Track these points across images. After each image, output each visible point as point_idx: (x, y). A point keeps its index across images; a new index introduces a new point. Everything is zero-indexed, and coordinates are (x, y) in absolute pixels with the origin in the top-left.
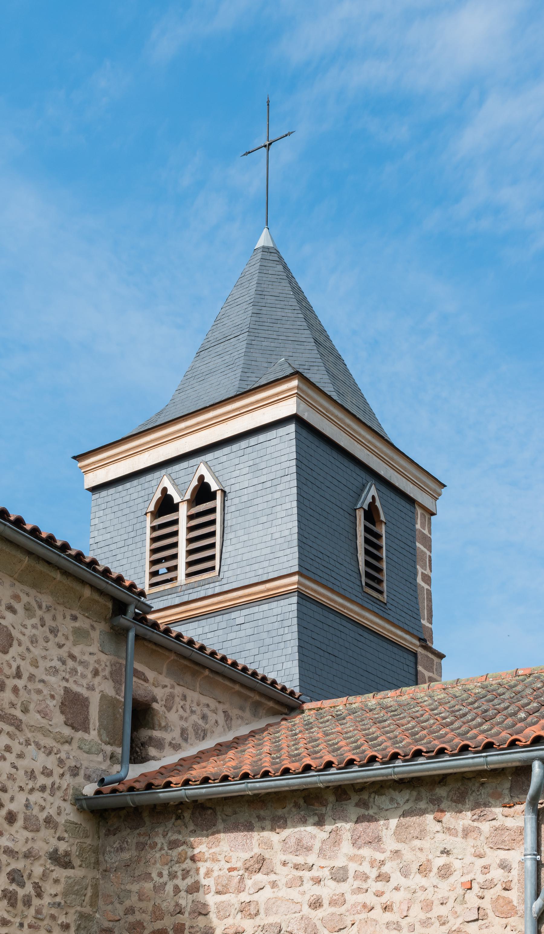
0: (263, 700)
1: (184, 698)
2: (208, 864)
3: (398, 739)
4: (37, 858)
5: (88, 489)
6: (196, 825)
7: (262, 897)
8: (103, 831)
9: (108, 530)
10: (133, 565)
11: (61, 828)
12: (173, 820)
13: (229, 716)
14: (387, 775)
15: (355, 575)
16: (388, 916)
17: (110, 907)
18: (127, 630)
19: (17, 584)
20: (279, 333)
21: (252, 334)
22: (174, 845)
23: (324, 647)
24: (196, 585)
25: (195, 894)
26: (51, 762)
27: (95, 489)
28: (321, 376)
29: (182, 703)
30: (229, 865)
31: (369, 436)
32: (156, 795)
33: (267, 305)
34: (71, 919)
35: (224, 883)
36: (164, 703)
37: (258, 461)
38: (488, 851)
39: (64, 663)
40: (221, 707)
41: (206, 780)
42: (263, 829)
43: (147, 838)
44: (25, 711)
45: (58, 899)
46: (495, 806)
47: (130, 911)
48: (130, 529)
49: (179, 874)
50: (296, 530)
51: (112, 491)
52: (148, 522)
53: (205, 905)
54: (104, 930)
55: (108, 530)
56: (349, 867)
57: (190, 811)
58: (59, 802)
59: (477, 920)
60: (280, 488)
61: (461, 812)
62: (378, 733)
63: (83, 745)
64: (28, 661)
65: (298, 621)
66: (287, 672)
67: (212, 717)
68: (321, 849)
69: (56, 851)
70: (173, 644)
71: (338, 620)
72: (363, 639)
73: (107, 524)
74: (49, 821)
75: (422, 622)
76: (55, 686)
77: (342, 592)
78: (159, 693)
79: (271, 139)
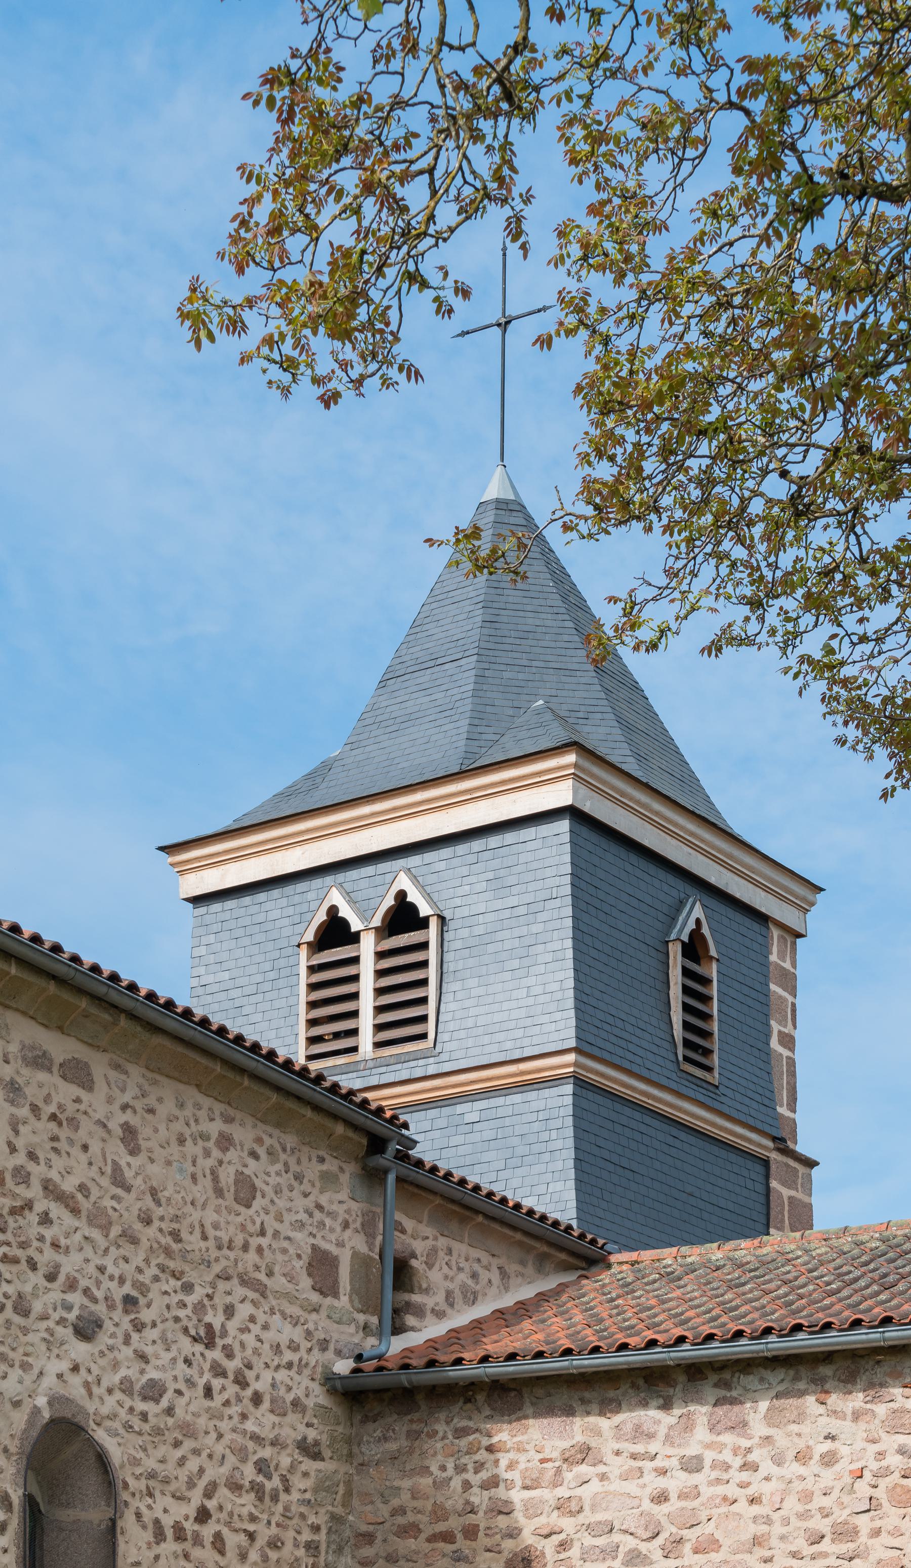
0: (552, 1251)
1: (450, 1252)
2: (511, 1455)
3: (768, 1309)
4: (284, 1447)
5: (187, 900)
6: (493, 1409)
7: (586, 1492)
8: (358, 1417)
9: (225, 966)
10: (274, 1024)
11: (309, 1413)
12: (460, 1403)
13: (505, 1272)
14: (757, 1352)
15: (667, 1045)
16: (756, 1509)
17: (369, 1508)
18: (386, 1172)
19: (259, 1124)
20: (531, 656)
21: (484, 658)
22: (461, 1433)
23: (615, 1159)
24: (392, 1061)
25: (493, 1490)
26: (297, 1334)
27: (197, 900)
28: (608, 730)
29: (447, 1258)
30: (541, 1456)
31: (691, 826)
32: (445, 1374)
33: (508, 606)
34: (321, 1519)
35: (534, 1476)
36: (424, 1259)
37: (502, 873)
38: (884, 1436)
39: (311, 1215)
40: (495, 1262)
41: (512, 1357)
42: (588, 1413)
43: (423, 1425)
44: (270, 1274)
45: (308, 1496)
46: (894, 1387)
47: (401, 1511)
48: (267, 966)
49: (470, 1467)
50: (571, 983)
51: (231, 904)
52: (303, 959)
53: (507, 1502)
54: (361, 1535)
55: (225, 966)
56: (705, 1456)
57: (485, 1394)
58: (306, 1382)
59: (868, 1511)
60: (541, 917)
61: (850, 1393)
62: (738, 1302)
63: (332, 1314)
64: (272, 1214)
65: (574, 1121)
66: (556, 1197)
67: (484, 1275)
68: (667, 1436)
69: (305, 1438)
70: (441, 1186)
71: (637, 1115)
72: (677, 1143)
73: (224, 956)
74: (296, 1403)
75: (779, 1109)
76: (302, 1244)
77: (645, 1073)
78: (419, 1246)
79: (511, 311)
